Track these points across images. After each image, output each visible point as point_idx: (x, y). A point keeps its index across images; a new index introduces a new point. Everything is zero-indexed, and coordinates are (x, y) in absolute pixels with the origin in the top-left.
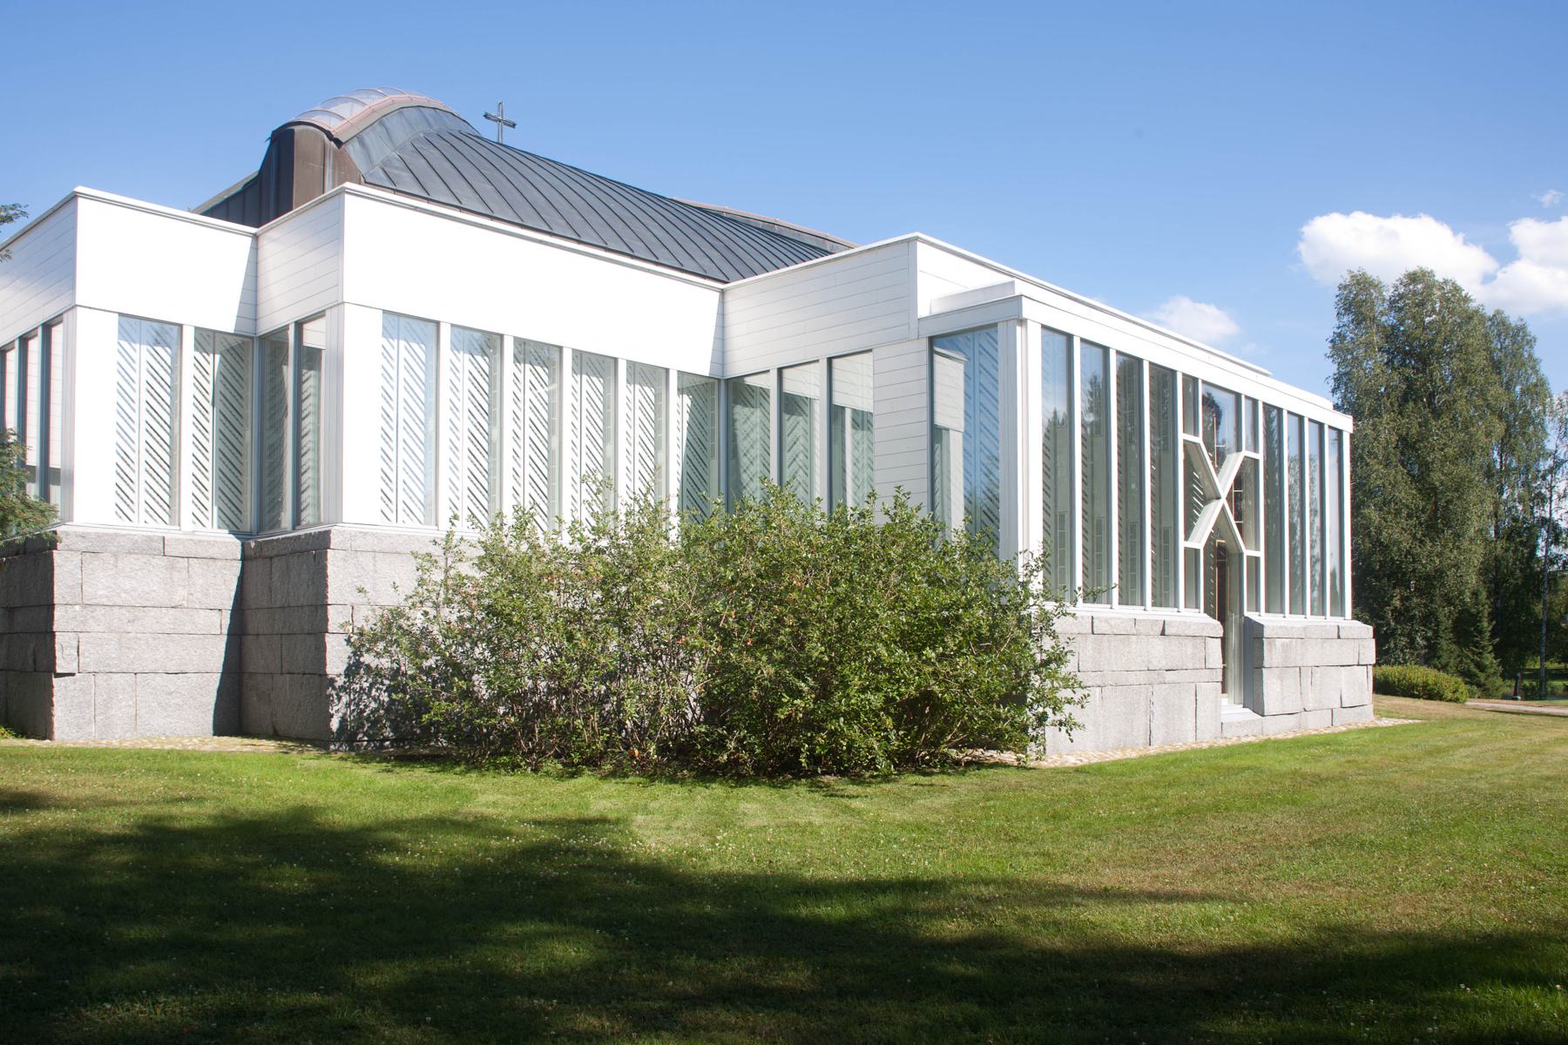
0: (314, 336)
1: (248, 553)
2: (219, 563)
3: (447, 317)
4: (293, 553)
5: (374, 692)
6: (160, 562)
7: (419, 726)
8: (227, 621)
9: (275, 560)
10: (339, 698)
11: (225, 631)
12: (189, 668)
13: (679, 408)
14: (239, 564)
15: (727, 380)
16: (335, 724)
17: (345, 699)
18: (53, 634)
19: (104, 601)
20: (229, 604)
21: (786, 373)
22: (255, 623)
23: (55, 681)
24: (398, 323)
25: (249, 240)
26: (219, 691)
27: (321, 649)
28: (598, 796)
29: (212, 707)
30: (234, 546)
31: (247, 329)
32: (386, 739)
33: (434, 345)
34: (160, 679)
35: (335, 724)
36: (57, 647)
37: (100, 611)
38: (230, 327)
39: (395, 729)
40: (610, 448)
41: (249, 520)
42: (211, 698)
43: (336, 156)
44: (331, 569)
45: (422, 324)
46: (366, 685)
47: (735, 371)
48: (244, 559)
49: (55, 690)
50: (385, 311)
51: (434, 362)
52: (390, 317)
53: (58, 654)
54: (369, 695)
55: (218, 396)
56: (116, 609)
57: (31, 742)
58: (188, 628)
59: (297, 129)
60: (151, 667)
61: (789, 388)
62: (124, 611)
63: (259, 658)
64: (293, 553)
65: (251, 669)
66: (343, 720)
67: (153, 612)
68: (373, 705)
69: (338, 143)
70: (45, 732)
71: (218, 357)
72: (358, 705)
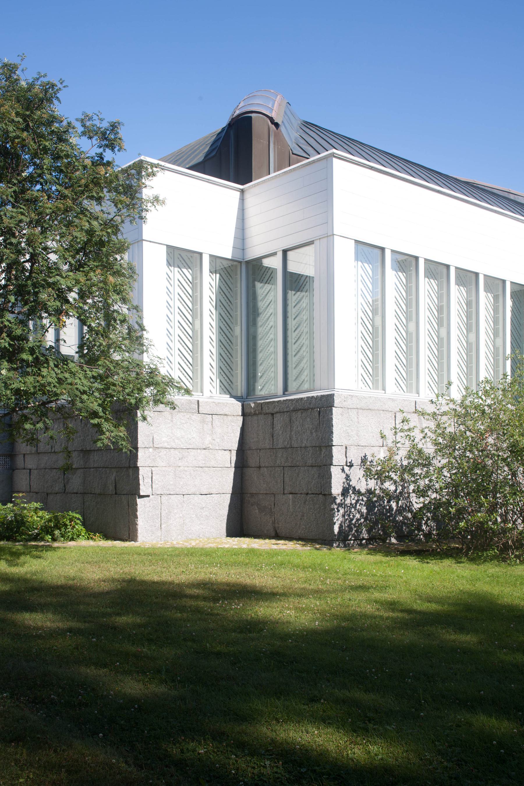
0: (302, 264)
1: (247, 411)
2: (230, 418)
3: (389, 245)
4: (295, 410)
5: (358, 507)
6: (196, 417)
7: (387, 529)
8: (234, 458)
9: (277, 417)
10: (338, 511)
11: (233, 465)
12: (214, 491)
13: (210, 283)
14: (241, 419)
15: (248, 262)
16: (336, 529)
17: (342, 511)
18: (137, 469)
19: (166, 445)
20: (235, 446)
21: (290, 254)
22: (253, 460)
23: (139, 501)
24: (370, 252)
25: (238, 194)
26: (230, 506)
27: (329, 476)
28: (215, 570)
29: (225, 517)
30: (237, 406)
31: (239, 257)
32: (363, 539)
33: (379, 264)
34: (197, 499)
35: (336, 529)
36: (141, 477)
37: (163, 452)
38: (228, 255)
39: (369, 531)
40: (412, 326)
41: (240, 386)
42: (225, 512)
43: (276, 136)
44: (336, 421)
45: (370, 249)
46: (354, 502)
47: (253, 253)
48: (244, 414)
49: (139, 507)
50: (357, 241)
51: (379, 277)
52: (360, 247)
53: (141, 482)
54: (355, 508)
55: (219, 303)
56: (172, 450)
57: (118, 543)
58: (213, 463)
59: (253, 115)
60: (192, 490)
61: (292, 268)
62: (176, 452)
63: (257, 483)
64: (295, 410)
65: (253, 490)
66: (341, 527)
67: (193, 452)
68: (358, 516)
69: (277, 125)
70: (131, 535)
71: (218, 275)
72: (349, 516)
